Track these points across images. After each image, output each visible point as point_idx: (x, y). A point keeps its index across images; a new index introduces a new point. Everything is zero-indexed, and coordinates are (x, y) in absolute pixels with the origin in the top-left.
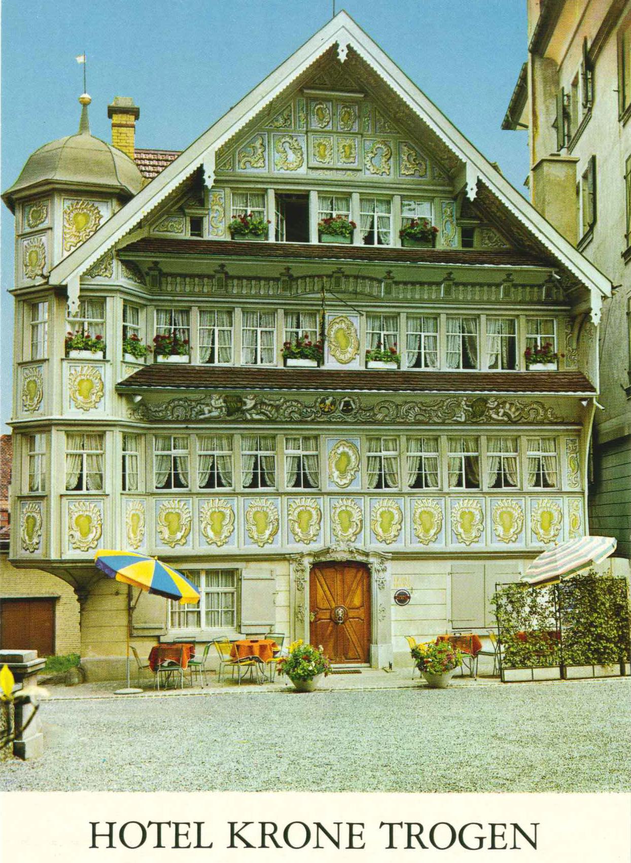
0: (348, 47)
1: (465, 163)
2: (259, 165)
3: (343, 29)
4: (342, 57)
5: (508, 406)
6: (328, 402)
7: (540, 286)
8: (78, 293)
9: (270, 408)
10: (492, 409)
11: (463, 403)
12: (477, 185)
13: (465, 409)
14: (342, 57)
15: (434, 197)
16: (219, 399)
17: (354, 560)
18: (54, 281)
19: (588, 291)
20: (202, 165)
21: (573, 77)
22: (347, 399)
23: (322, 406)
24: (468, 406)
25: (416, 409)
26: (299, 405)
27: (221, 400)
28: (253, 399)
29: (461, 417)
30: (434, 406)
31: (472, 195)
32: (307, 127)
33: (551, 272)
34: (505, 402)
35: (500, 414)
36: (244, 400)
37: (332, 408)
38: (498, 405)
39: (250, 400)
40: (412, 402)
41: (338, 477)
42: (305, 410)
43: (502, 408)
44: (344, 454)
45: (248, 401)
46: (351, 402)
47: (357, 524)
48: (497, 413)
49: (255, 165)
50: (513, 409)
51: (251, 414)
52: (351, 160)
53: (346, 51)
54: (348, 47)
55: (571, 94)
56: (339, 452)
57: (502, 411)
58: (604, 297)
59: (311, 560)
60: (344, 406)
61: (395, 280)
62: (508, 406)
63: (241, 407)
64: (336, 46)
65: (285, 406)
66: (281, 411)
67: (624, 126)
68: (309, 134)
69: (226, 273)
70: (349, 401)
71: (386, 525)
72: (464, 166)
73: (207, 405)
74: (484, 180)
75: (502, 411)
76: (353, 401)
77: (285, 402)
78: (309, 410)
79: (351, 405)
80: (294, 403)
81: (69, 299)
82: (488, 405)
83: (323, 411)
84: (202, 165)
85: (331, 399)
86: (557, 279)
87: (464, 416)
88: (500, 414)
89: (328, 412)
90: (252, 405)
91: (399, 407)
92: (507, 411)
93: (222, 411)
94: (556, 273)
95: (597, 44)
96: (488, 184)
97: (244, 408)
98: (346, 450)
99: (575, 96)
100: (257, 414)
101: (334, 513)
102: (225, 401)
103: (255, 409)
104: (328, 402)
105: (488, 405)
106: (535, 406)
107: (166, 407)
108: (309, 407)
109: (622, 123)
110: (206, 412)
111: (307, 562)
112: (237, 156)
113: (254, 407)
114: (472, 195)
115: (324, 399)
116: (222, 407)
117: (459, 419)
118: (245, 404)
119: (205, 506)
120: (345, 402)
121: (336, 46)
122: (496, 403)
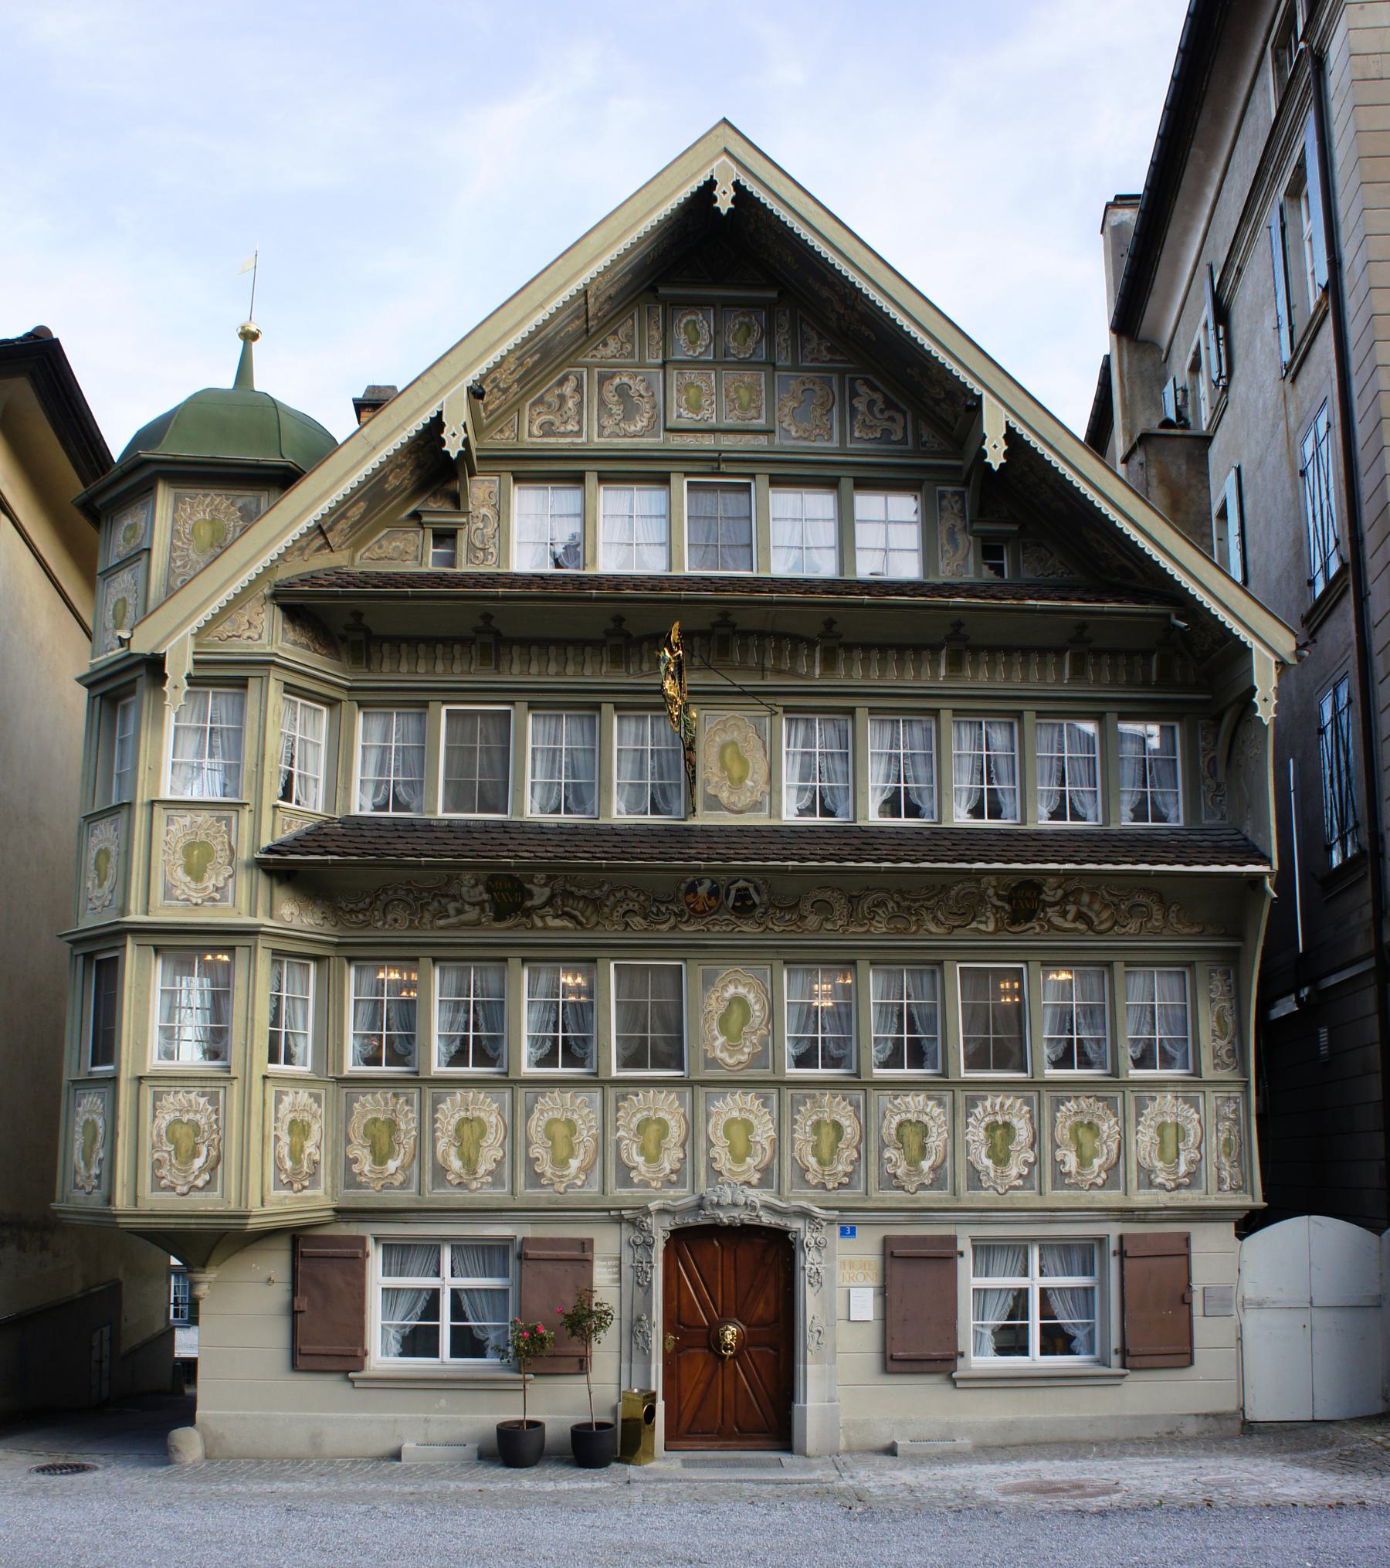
0: (737, 185)
1: (981, 396)
2: (569, 428)
3: (724, 158)
4: (724, 202)
5: (1085, 898)
6: (702, 890)
7: (1147, 654)
8: (188, 667)
9: (581, 904)
10: (1052, 905)
11: (991, 892)
12: (1005, 437)
13: (994, 906)
14: (724, 202)
15: (922, 481)
16: (476, 885)
17: (756, 1222)
18: (141, 646)
19: (1245, 651)
20: (440, 414)
21: (1190, 357)
22: (741, 884)
23: (690, 898)
24: (1000, 898)
25: (891, 904)
26: (642, 898)
27: (481, 888)
28: (545, 885)
29: (986, 923)
30: (929, 899)
31: (995, 455)
32: (665, 355)
33: (1167, 617)
34: (1079, 891)
35: (1070, 916)
36: (528, 886)
37: (713, 902)
38: (1065, 896)
39: (541, 886)
40: (880, 889)
41: (724, 1048)
42: (654, 910)
43: (1074, 903)
44: (739, 1001)
45: (535, 890)
46: (752, 891)
47: (764, 1149)
48: (1064, 914)
49: (562, 429)
50: (1096, 907)
51: (542, 917)
52: (753, 413)
53: (732, 193)
54: (737, 185)
55: (1188, 387)
56: (727, 995)
57: (1072, 909)
58: (1282, 664)
59: (668, 1223)
60: (736, 900)
61: (842, 640)
62: (1085, 898)
63: (523, 902)
64: (711, 184)
65: (612, 898)
66: (606, 910)
67: (1293, 381)
68: (669, 367)
69: (497, 633)
70: (746, 889)
71: (825, 1152)
72: (979, 398)
73: (454, 898)
74: (1021, 429)
75: (1072, 909)
76: (757, 889)
77: (612, 892)
78: (663, 909)
79: (751, 898)
80: (630, 893)
81: (168, 682)
82: (1043, 897)
83: (693, 910)
84: (440, 414)
85: (707, 884)
86: (1180, 629)
87: (992, 919)
88: (1070, 916)
89: (704, 911)
90: (543, 899)
91: (855, 901)
92: (1085, 910)
93: (483, 910)
94: (1178, 618)
95: (1233, 265)
96: (1028, 436)
97: (529, 904)
98: (741, 990)
99: (1195, 387)
100: (556, 917)
101: (716, 1124)
102: (489, 890)
103: (552, 906)
104: (702, 890)
105: (1043, 897)
106: (1142, 899)
107: (371, 903)
108: (663, 903)
109: (1289, 379)
110: (452, 912)
111: (659, 1231)
112: (527, 413)
113: (549, 902)
114: (995, 455)
115: (693, 883)
116: (484, 901)
117: (982, 927)
118: (530, 895)
119: (178, 892)
120: (738, 890)
121: (711, 184)
122: (1060, 892)
